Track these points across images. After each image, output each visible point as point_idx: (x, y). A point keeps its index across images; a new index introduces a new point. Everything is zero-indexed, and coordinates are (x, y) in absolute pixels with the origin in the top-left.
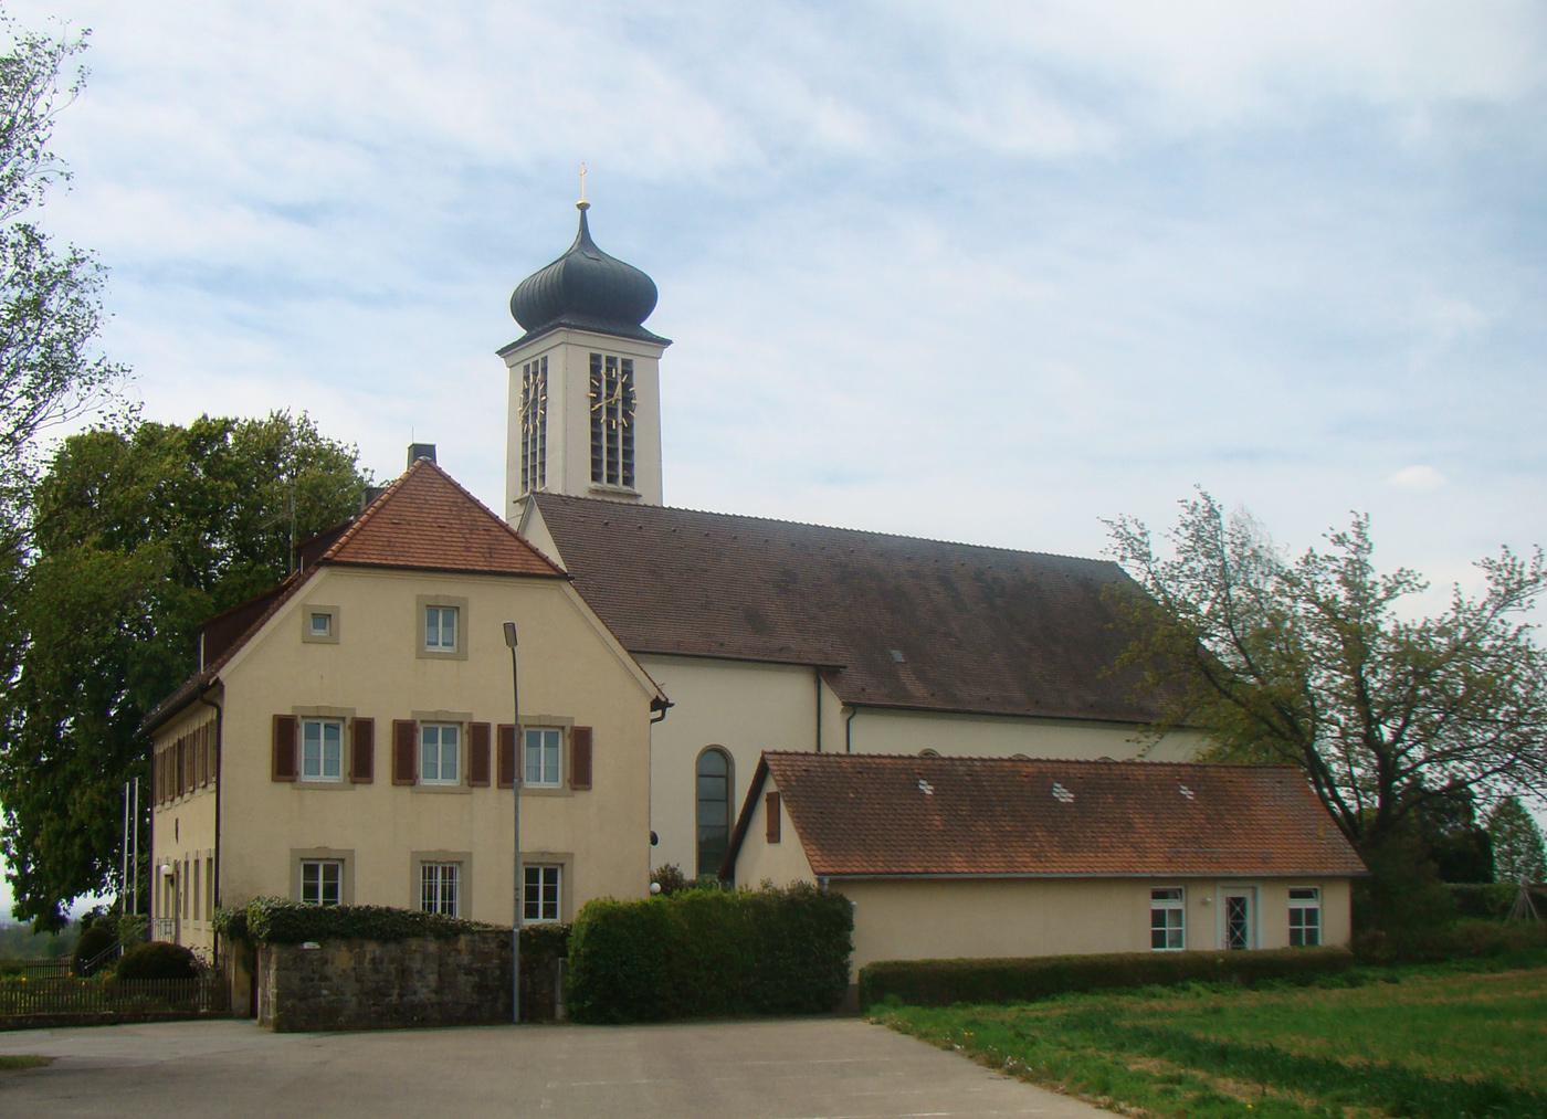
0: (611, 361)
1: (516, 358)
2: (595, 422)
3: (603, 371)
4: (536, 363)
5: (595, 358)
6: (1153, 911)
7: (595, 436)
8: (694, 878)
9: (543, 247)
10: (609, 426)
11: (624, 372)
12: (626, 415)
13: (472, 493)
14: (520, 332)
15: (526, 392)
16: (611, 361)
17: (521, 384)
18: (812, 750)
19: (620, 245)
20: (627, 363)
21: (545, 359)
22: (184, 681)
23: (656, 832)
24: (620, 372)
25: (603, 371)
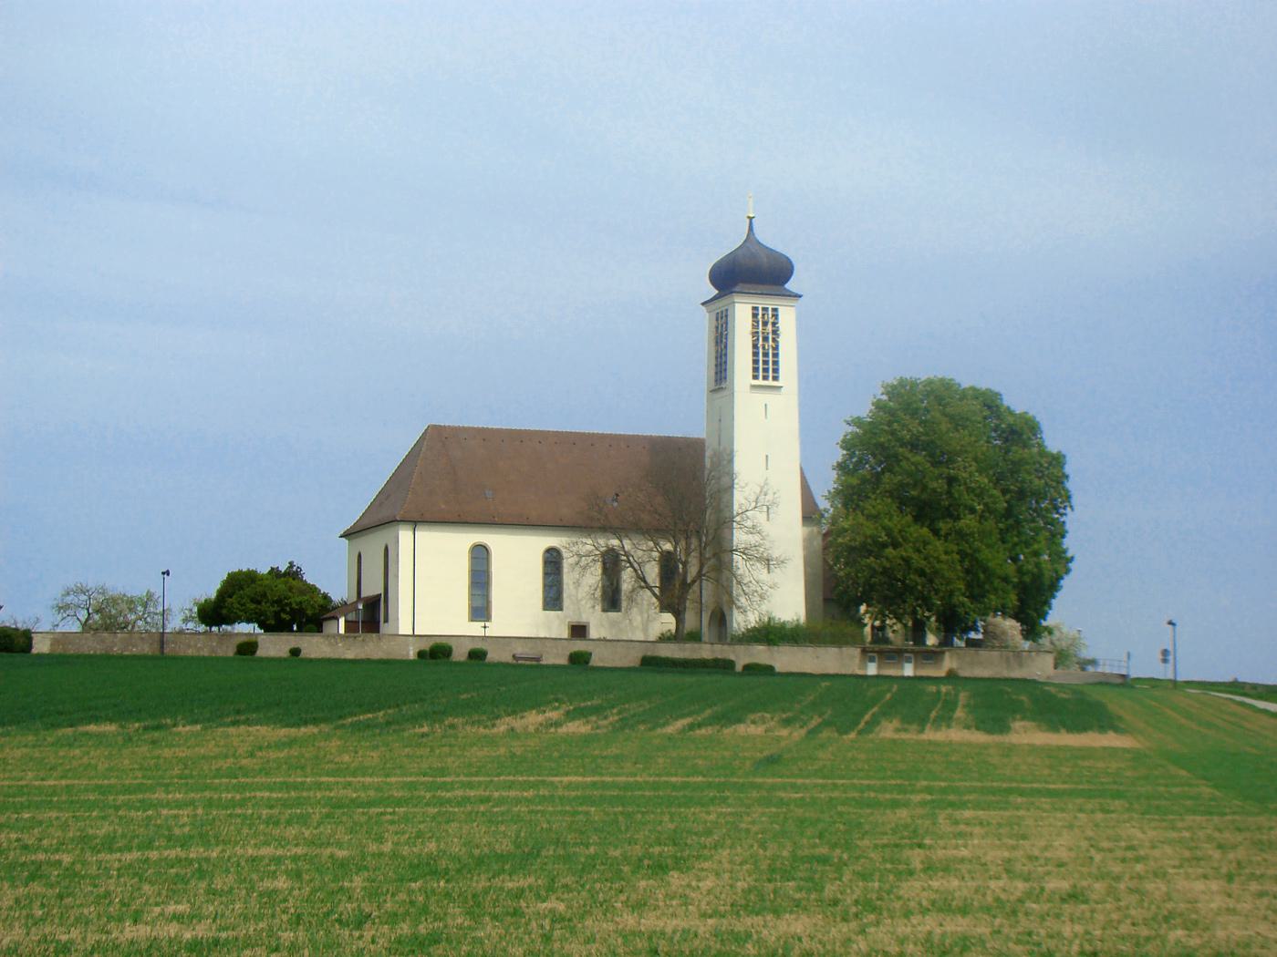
0: (765, 309)
1: (713, 306)
2: (755, 346)
3: (760, 316)
4: (722, 312)
5: (755, 309)
6: (561, 609)
7: (755, 354)
8: (803, 619)
9: (727, 244)
10: (764, 348)
11: (773, 316)
12: (774, 340)
13: (653, 435)
14: (716, 292)
15: (717, 328)
16: (765, 309)
17: (714, 323)
18: (411, 633)
19: (771, 238)
20: (775, 310)
21: (727, 310)
22: (535, 859)
23: (1075, 559)
24: (770, 316)
25: (760, 316)
